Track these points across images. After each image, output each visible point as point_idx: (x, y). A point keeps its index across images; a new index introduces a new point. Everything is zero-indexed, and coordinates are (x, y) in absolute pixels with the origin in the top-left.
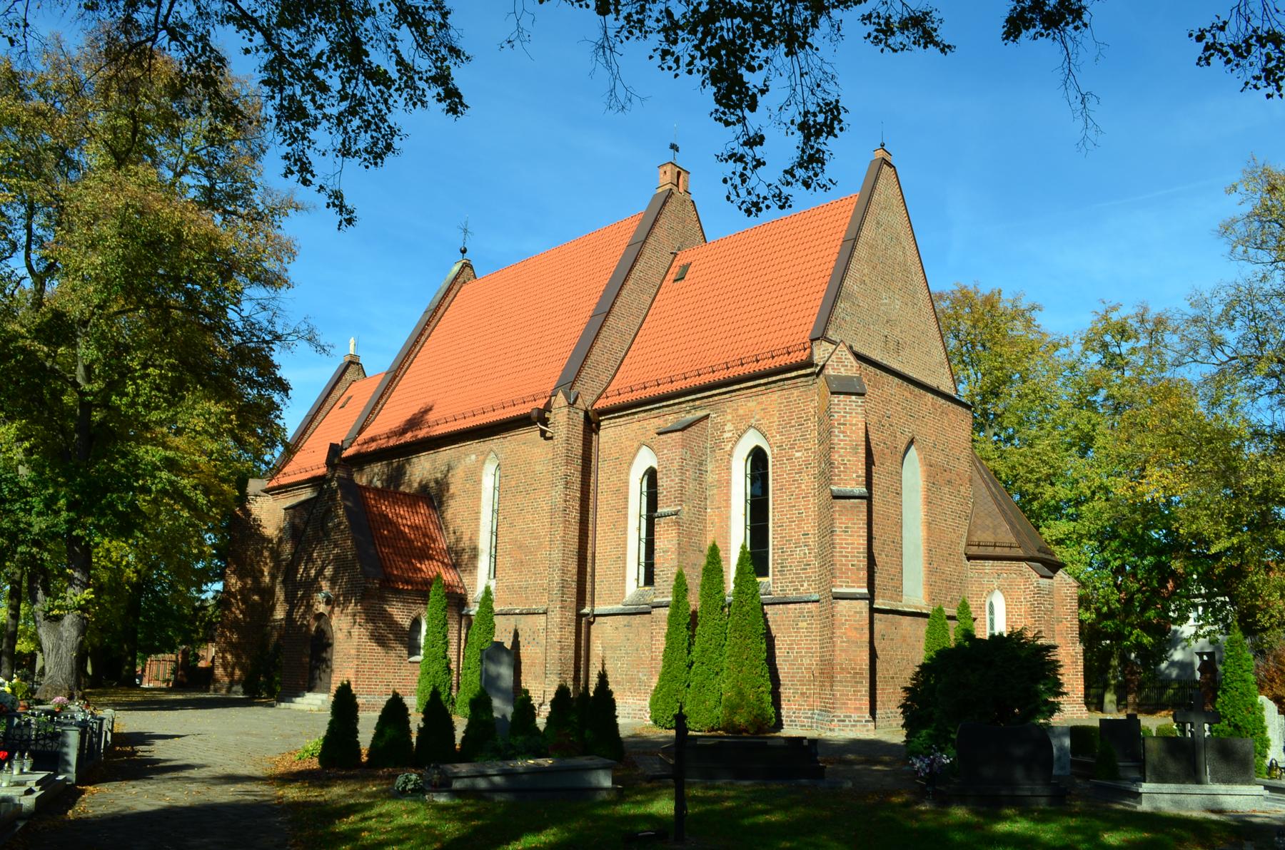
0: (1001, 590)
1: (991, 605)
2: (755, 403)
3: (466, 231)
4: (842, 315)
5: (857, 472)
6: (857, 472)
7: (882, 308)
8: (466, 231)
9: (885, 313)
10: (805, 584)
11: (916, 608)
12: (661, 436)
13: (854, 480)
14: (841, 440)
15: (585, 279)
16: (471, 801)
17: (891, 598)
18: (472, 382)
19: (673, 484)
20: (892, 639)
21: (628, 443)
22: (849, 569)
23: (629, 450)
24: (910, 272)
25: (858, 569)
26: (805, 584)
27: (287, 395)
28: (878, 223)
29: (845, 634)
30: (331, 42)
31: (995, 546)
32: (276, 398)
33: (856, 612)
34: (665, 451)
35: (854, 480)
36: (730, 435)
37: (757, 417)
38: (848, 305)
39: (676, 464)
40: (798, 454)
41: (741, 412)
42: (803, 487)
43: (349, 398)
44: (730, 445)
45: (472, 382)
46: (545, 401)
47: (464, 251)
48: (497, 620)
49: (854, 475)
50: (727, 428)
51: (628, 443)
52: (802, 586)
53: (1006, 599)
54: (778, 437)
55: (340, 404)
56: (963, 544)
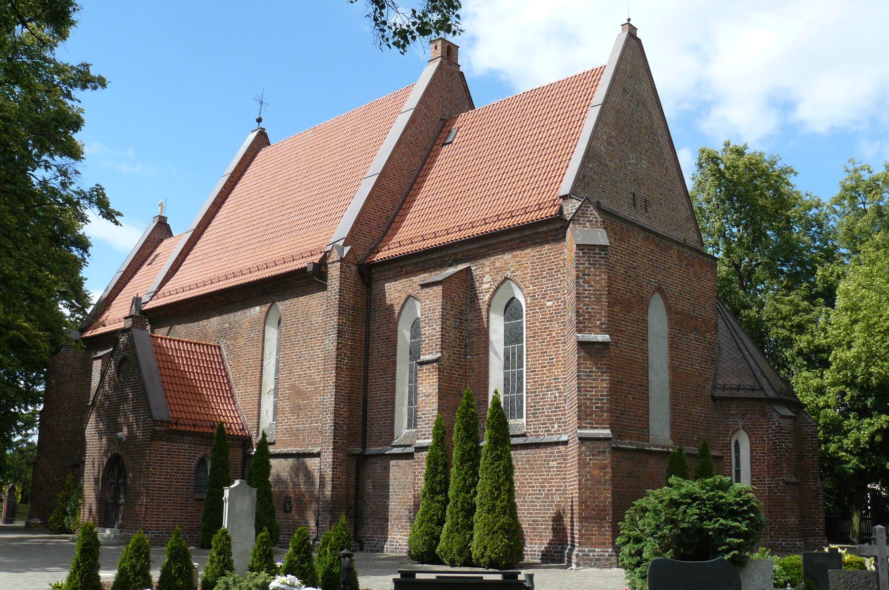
0: (745, 430)
1: (737, 444)
2: (510, 256)
3: (262, 103)
4: (590, 174)
5: (600, 320)
6: (600, 320)
7: (629, 167)
8: (262, 103)
9: (632, 172)
10: (556, 426)
11: (663, 447)
12: (427, 290)
13: (597, 327)
14: (586, 290)
15: (363, 144)
16: (705, 527)
17: (638, 438)
18: (259, 240)
19: (434, 332)
20: (638, 477)
21: (397, 295)
22: (593, 412)
23: (397, 301)
24: (656, 135)
25: (602, 411)
26: (556, 426)
27: (87, 252)
28: (624, 90)
29: (589, 472)
30: (779, 176)
31: (739, 389)
32: (76, 252)
33: (599, 452)
34: (428, 302)
35: (597, 327)
36: (488, 286)
37: (512, 269)
38: (595, 165)
39: (437, 314)
40: (549, 304)
41: (498, 265)
42: (554, 334)
43: (157, 256)
44: (488, 295)
45: (259, 240)
46: (320, 256)
47: (259, 120)
48: (273, 462)
49: (598, 323)
50: (485, 280)
51: (397, 295)
52: (553, 427)
53: (750, 438)
54: (531, 288)
55: (148, 262)
56: (709, 387)
